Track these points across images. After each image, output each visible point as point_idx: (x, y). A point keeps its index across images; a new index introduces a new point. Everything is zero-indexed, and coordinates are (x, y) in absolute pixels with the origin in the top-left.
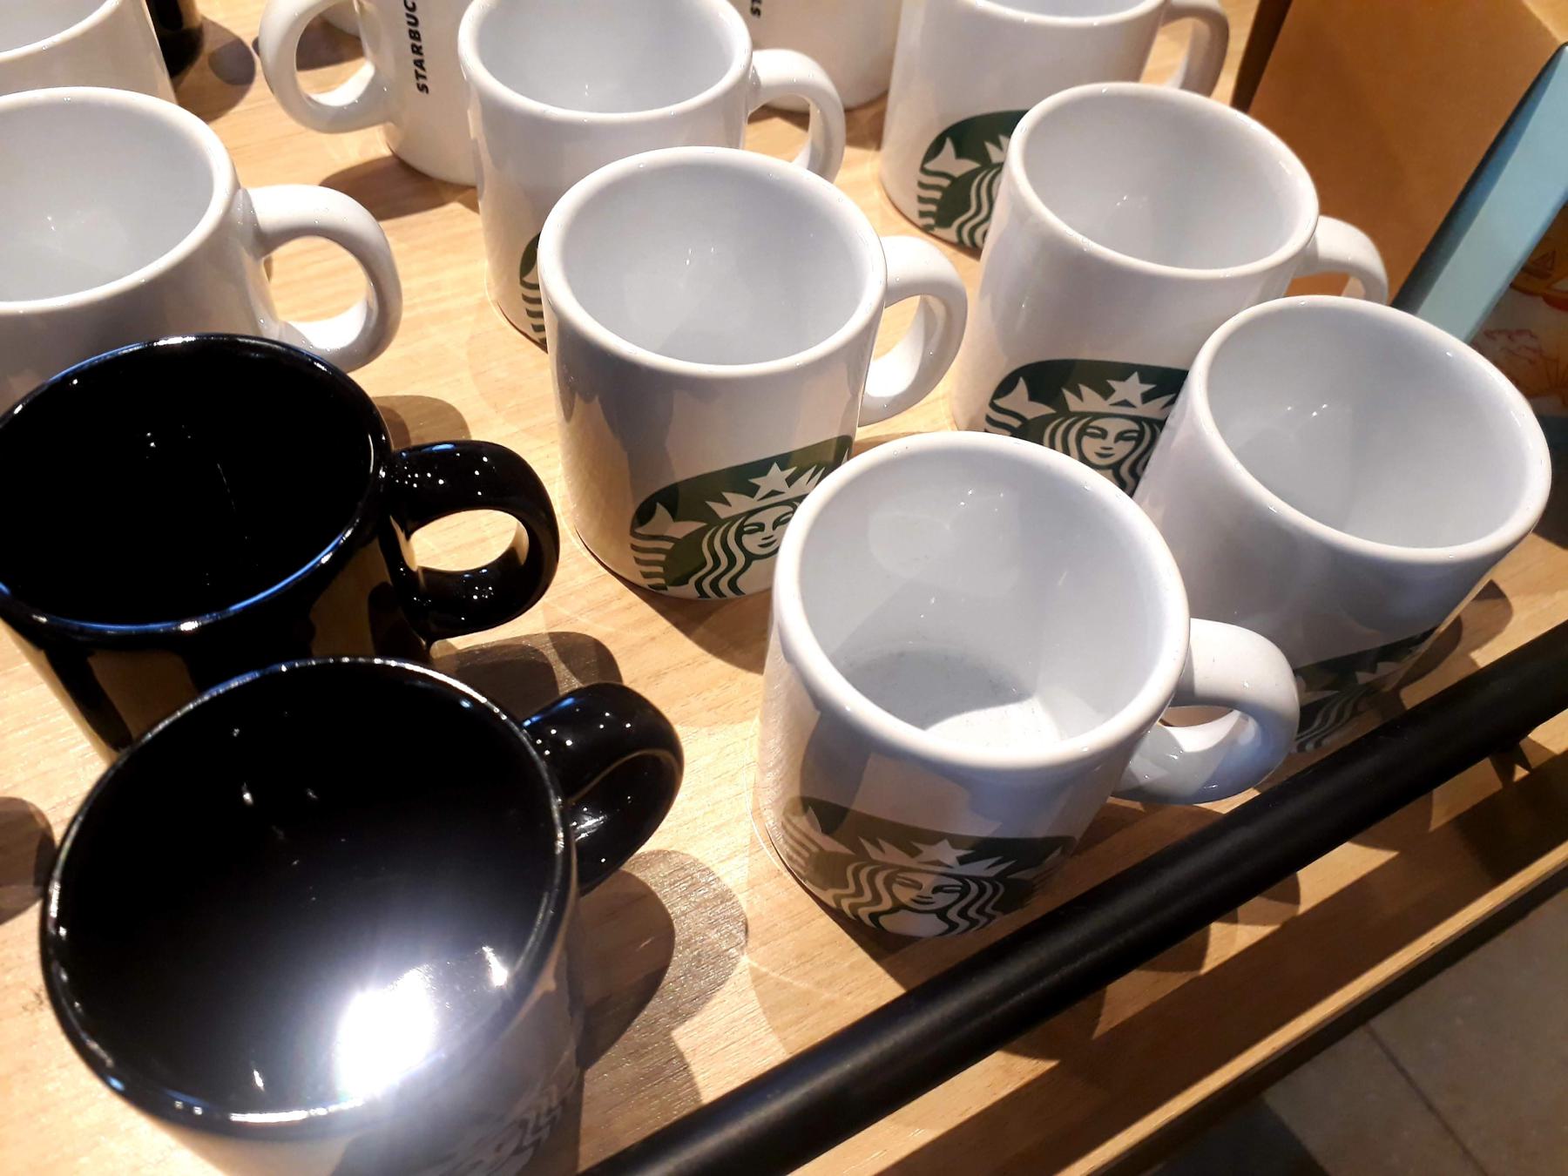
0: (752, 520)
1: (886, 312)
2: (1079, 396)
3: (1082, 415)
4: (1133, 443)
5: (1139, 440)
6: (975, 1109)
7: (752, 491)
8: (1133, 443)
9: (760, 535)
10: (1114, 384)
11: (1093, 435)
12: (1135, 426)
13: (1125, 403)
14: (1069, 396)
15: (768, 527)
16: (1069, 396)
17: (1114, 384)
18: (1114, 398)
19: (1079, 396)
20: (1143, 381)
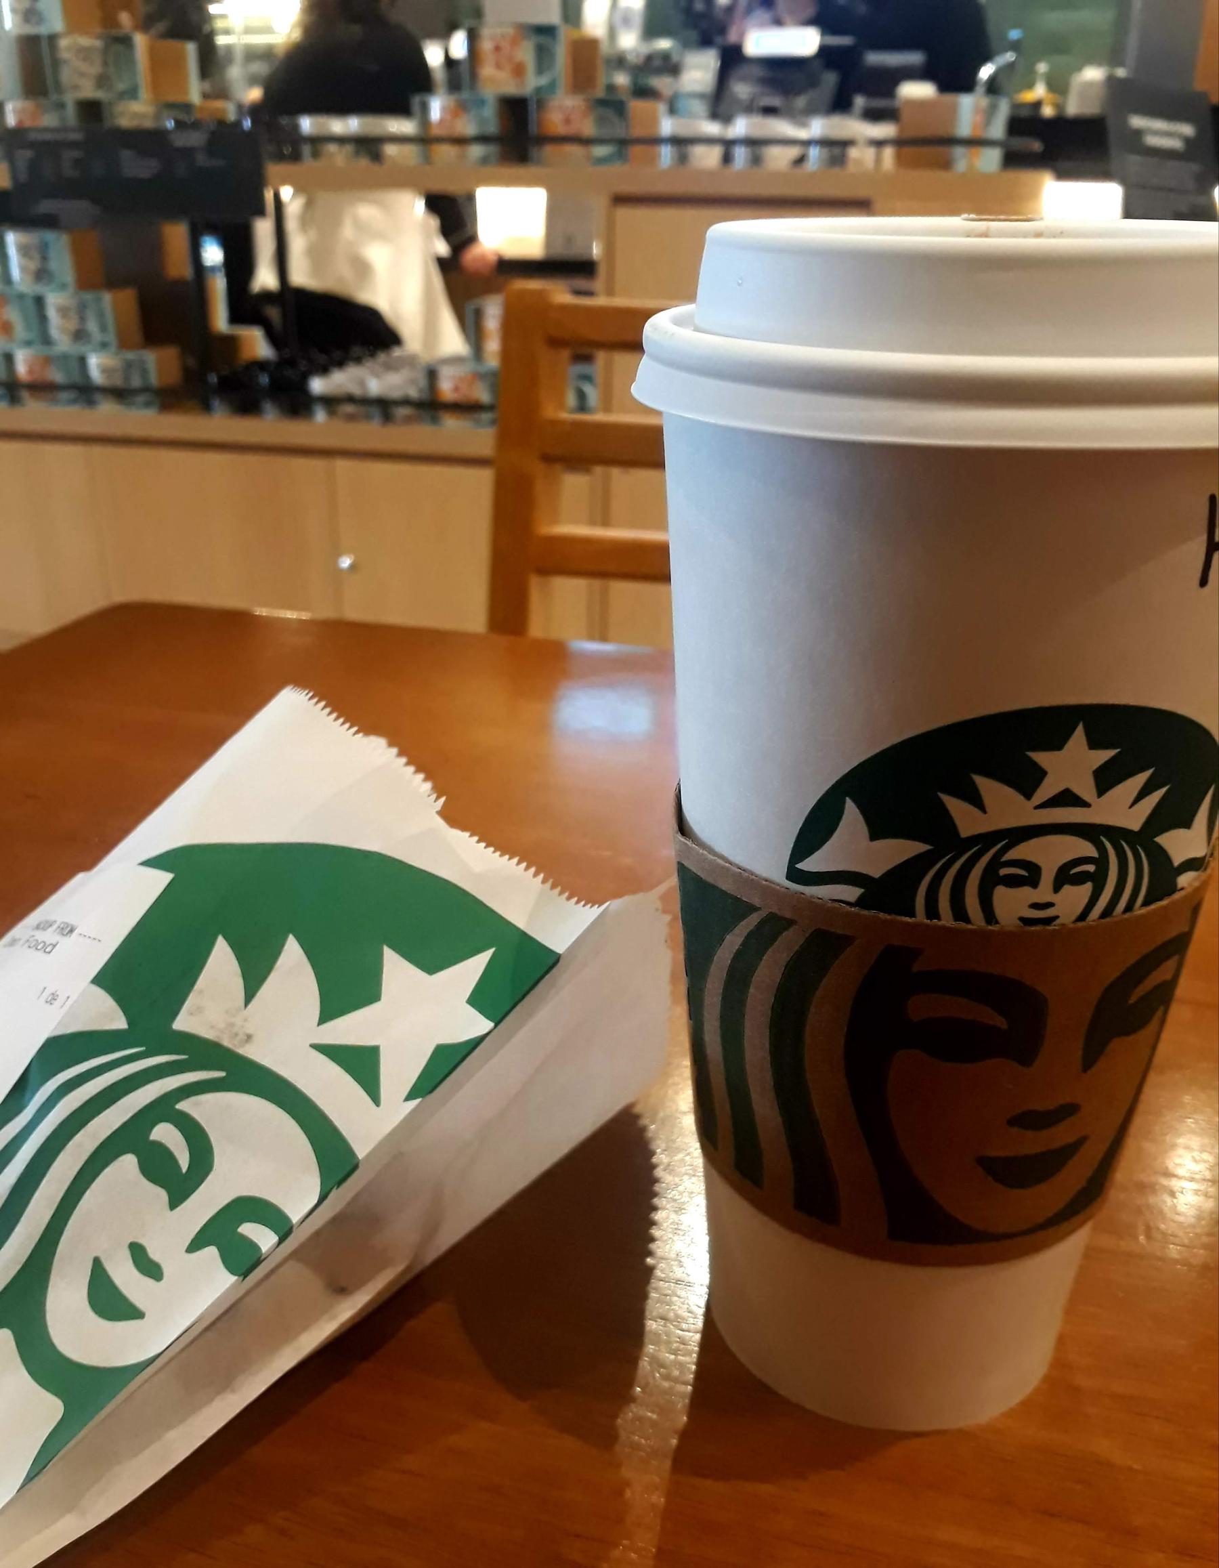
0: (1021, 851)
1: (334, 1190)
2: (975, 799)
3: (987, 840)
4: (1088, 888)
5: (1098, 881)
6: (338, 1123)
7: (1026, 780)
8: (1088, 888)
9: (1027, 894)
10: (1042, 758)
11: (1013, 882)
12: (1089, 850)
13: (1067, 798)
14: (956, 807)
15: (1047, 878)
16: (956, 807)
17: (1042, 758)
18: (1046, 790)
19: (975, 799)
20: (1094, 743)
